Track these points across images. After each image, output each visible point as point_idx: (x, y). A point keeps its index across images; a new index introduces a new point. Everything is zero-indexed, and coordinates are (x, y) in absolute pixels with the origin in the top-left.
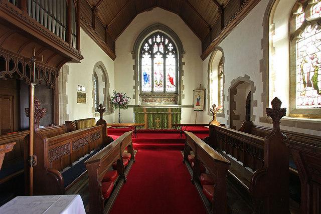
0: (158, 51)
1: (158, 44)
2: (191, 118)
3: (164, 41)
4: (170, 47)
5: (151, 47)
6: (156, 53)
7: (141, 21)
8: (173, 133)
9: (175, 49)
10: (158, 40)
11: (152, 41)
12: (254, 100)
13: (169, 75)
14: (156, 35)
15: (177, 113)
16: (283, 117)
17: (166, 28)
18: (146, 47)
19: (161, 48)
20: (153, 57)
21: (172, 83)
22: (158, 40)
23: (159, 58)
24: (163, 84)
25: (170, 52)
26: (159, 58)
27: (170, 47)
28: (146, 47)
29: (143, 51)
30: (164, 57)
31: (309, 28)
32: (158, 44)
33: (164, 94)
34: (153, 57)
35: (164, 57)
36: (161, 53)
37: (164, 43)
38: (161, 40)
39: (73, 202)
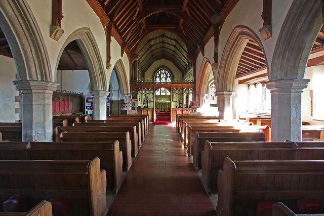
1: (163, 74)
4: (169, 75)
5: (160, 75)
7: (156, 64)
8: (45, 115)
9: (170, 76)
10: (163, 71)
12: (18, 114)
14: (162, 70)
15: (170, 104)
16: (214, 90)
17: (166, 67)
18: (158, 75)
19: (165, 76)
22: (163, 71)
27: (169, 75)
28: (158, 75)
29: (156, 77)
32: (163, 74)
33: (165, 96)
39: (16, 69)
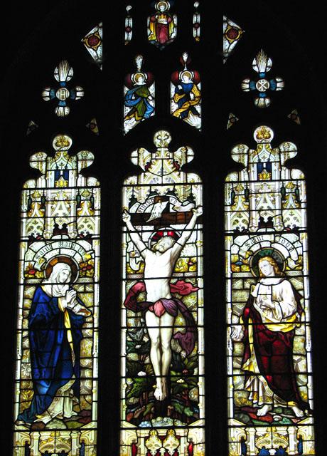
0: (163, 119)
1: (162, 67)
2: (172, 356)
3: (213, 35)
5: (103, 88)
6: (143, 137)
11: (112, 42)
13: (250, 313)
20: (112, 170)
21: (284, 384)
23: (161, 173)
24: (200, 391)
25: (263, 117)
26: (161, 173)
30: (213, 166)
31: (90, 386)
32: (162, 67)
34: (112, 170)
35: (213, 166)
36: (181, 135)
37: (206, 58)
38: (185, 27)
